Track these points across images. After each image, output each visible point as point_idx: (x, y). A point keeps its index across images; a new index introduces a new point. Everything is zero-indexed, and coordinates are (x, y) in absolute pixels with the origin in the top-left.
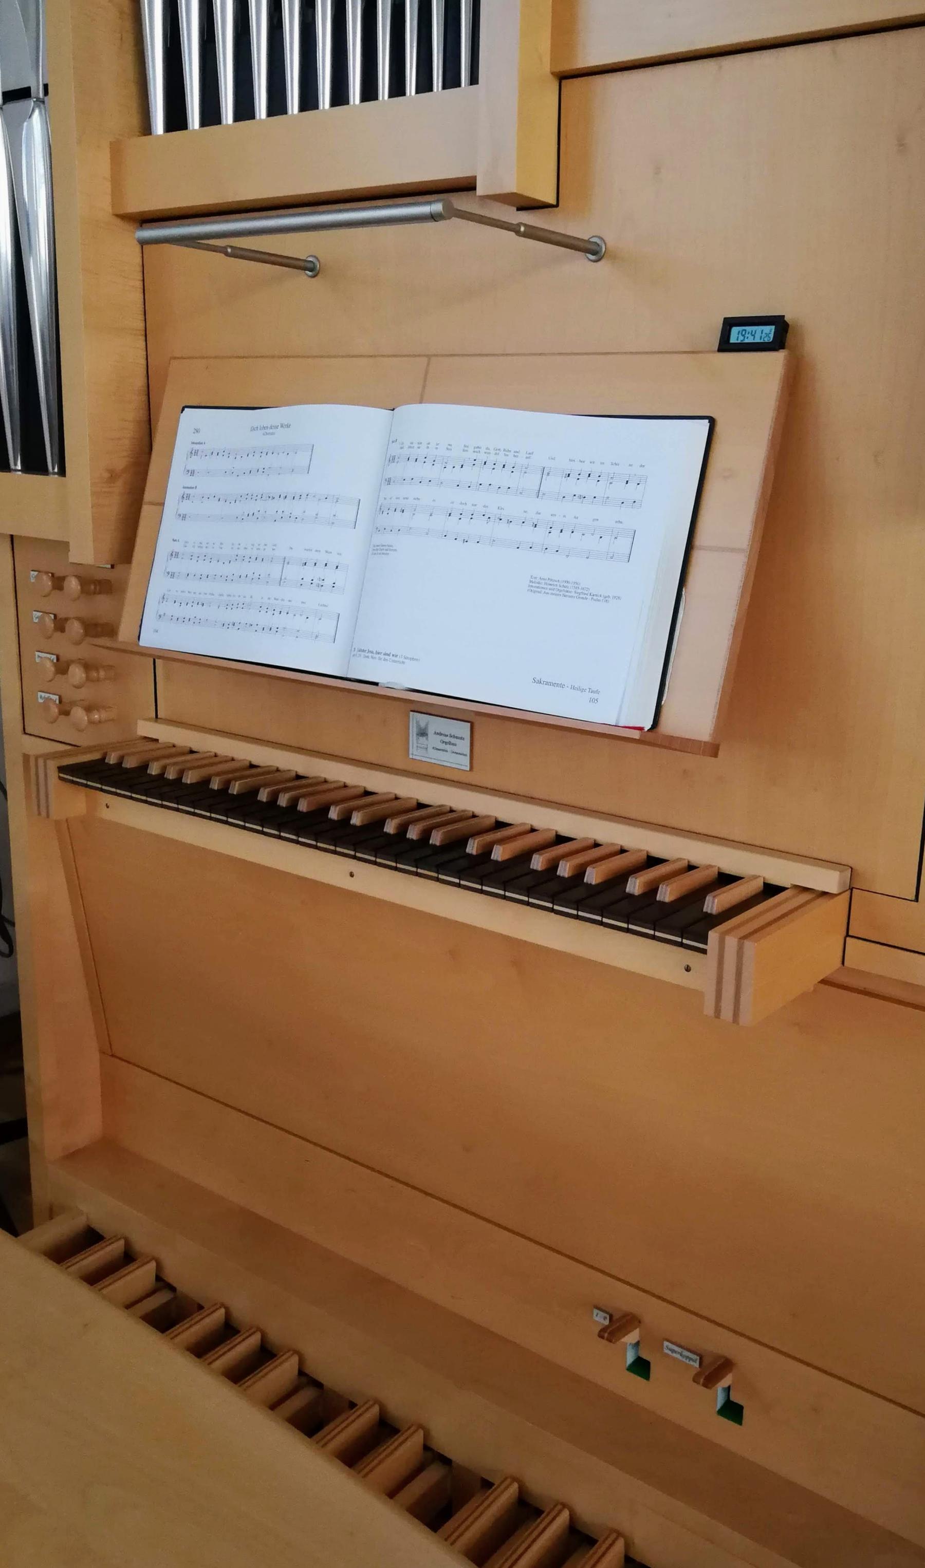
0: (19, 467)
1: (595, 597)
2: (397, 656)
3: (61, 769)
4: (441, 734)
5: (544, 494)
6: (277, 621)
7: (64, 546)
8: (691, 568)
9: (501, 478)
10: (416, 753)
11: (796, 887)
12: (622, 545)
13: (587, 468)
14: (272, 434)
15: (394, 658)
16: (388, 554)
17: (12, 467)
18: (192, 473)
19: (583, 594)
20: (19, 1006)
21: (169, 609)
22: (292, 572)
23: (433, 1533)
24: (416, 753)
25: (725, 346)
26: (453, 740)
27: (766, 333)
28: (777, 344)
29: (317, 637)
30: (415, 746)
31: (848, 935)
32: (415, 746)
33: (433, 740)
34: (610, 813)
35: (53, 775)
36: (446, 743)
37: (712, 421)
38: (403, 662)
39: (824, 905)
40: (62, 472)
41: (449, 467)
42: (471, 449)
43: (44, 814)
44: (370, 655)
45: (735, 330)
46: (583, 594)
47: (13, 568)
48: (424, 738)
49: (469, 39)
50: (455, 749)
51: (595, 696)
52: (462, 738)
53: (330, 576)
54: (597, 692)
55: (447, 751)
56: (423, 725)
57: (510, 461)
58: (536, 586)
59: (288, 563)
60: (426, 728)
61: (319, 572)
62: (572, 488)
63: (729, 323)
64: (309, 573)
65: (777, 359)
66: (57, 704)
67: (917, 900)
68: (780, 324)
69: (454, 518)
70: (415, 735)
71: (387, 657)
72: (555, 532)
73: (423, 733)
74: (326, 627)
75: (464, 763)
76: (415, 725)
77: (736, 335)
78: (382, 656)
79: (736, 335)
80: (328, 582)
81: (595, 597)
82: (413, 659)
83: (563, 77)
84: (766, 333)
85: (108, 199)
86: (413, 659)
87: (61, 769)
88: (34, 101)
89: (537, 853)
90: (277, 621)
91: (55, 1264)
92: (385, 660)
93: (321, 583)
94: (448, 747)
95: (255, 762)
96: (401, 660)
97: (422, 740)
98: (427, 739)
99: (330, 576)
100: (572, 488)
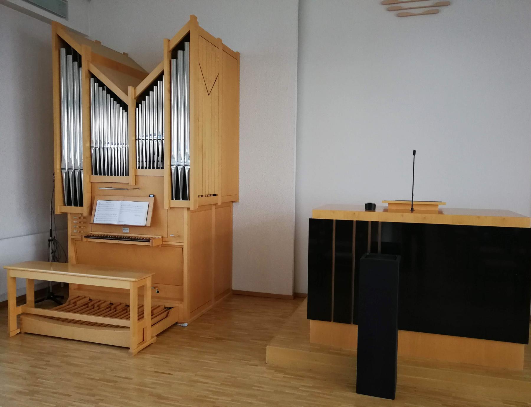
3: (84, 236)
20: (150, 73)
21: (97, 219)
22: (112, 215)
23: (349, 325)
25: (150, 197)
27: (153, 196)
28: (154, 197)
31: (163, 241)
33: (125, 230)
34: (408, 17)
35: (84, 237)
47: (89, 126)
63: (150, 195)
68: (154, 195)
75: (128, 232)
83: (135, 176)
85: (88, 180)
87: (84, 236)
89: (52, 309)
91: (8, 317)
99: (116, 215)
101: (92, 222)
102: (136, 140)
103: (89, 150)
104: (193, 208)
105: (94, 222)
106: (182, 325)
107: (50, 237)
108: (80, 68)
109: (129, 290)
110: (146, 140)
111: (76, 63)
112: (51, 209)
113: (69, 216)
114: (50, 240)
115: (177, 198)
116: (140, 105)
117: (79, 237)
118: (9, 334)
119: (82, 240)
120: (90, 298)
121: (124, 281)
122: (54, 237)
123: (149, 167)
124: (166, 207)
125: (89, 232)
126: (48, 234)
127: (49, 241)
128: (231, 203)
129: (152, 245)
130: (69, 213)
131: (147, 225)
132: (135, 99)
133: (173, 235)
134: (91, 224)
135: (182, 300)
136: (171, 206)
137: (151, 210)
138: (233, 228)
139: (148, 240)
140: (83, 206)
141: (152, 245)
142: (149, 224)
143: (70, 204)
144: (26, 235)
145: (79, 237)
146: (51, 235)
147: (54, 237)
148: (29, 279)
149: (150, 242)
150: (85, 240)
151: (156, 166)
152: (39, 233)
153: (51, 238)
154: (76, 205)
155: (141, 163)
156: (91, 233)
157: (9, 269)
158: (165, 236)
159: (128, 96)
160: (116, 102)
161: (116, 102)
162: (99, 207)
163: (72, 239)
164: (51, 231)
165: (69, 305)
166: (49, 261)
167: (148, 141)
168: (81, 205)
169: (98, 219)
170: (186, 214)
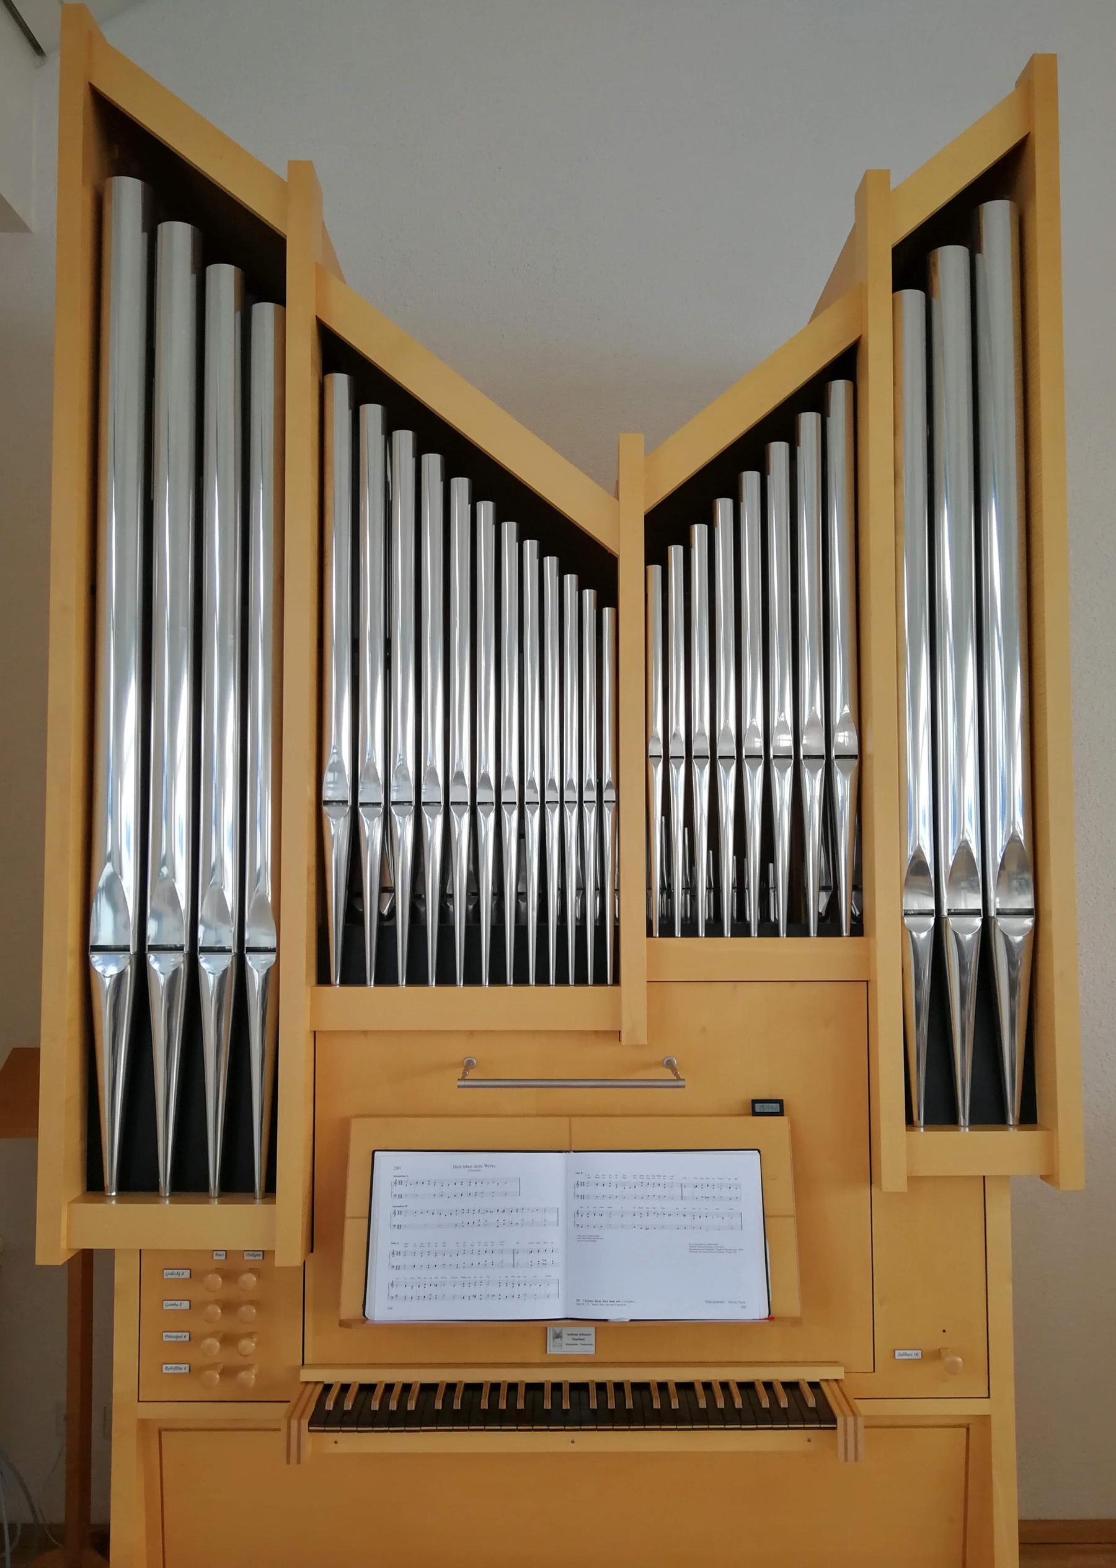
1: (729, 1251)
2: (619, 1302)
4: (572, 1334)
5: (685, 1198)
8: (306, 1221)
9: (658, 1191)
15: (618, 1303)
18: (400, 1196)
19: (721, 1250)
26: (582, 1337)
27: (775, 1107)
28: (781, 1113)
29: (548, 1296)
30: (551, 1345)
32: (551, 1345)
33: (566, 1339)
36: (577, 1339)
38: (625, 1305)
41: (627, 1188)
42: (638, 1177)
44: (598, 1303)
46: (721, 1250)
48: (559, 1339)
49: (110, 1031)
50: (583, 1342)
51: (743, 1305)
52: (590, 1335)
53: (549, 1257)
54: (744, 1302)
55: (577, 1344)
57: (662, 1181)
58: (693, 1249)
59: (518, 1253)
60: (561, 1333)
63: (754, 1102)
66: (296, 1372)
67: (874, 1371)
68: (780, 1102)
69: (638, 1216)
70: (552, 1337)
71: (612, 1303)
73: (558, 1336)
74: (553, 1289)
76: (552, 1332)
77: (758, 1108)
78: (608, 1303)
79: (758, 1108)
80: (549, 1261)
81: (729, 1251)
84: (775, 1107)
88: (204, 961)
92: (611, 1305)
93: (545, 1262)
94: (578, 1342)
96: (624, 1303)
97: (558, 1340)
98: (562, 1339)
99: (549, 1257)
116: (675, 553)
136: (923, 1170)
137: (785, 1201)
142: (791, 1305)
163: (143, 1425)
169: (408, 1292)
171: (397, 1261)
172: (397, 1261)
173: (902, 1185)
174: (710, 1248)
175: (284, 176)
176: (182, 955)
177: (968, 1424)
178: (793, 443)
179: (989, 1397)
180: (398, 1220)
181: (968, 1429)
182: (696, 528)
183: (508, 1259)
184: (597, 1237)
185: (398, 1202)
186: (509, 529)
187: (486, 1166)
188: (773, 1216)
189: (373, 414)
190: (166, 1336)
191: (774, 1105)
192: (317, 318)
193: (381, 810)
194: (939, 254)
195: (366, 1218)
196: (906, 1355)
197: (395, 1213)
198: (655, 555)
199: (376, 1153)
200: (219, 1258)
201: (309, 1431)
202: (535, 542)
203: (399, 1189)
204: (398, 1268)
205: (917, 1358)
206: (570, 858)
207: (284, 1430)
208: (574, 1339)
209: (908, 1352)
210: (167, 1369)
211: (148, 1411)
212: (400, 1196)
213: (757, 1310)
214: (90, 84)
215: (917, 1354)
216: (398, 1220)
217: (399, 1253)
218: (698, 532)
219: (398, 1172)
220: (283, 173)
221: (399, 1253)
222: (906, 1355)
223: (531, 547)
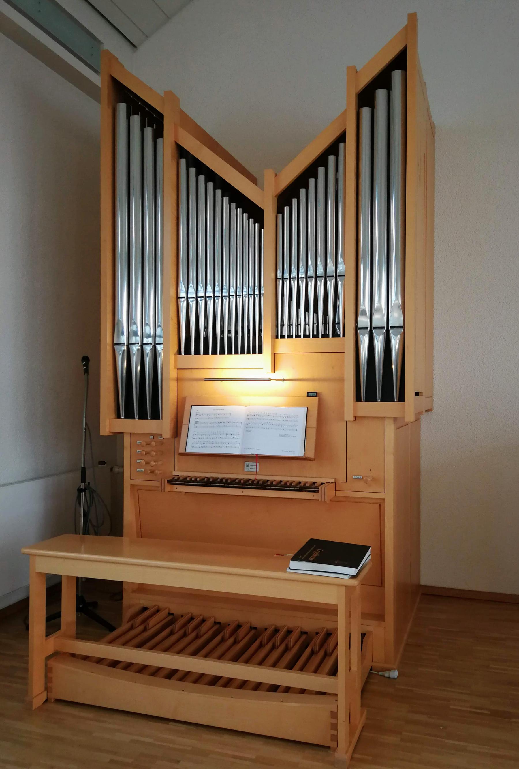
0: (137, 418)
3: (168, 481)
6: (228, 445)
7: (161, 435)
10: (246, 470)
11: (327, 483)
12: (295, 428)
13: (287, 416)
14: (219, 411)
16: (251, 431)
17: (135, 418)
18: (197, 418)
19: (289, 436)
22: (228, 436)
24: (246, 470)
25: (308, 396)
27: (315, 394)
28: (316, 396)
31: (335, 490)
33: (250, 467)
35: (166, 480)
37: (307, 408)
39: (333, 484)
40: (162, 420)
43: (163, 490)
45: (309, 394)
46: (289, 436)
56: (248, 464)
60: (248, 465)
61: (235, 436)
62: (284, 419)
63: (308, 393)
64: (232, 436)
65: (317, 398)
68: (316, 393)
72: (283, 426)
73: (248, 466)
77: (309, 394)
79: (309, 394)
80: (237, 437)
82: (258, 449)
84: (315, 394)
86: (258, 449)
87: (168, 481)
90: (228, 445)
94: (254, 468)
95: (207, 477)
99: (237, 436)
100: (284, 419)
101: (181, 450)
102: (276, 279)
103: (175, 303)
104: (352, 419)
105: (188, 451)
106: (387, 675)
107: (82, 482)
108: (159, 140)
109: (336, 606)
110: (199, 299)
111: (149, 131)
112: (84, 426)
113: (127, 440)
114: (82, 489)
115: (371, 397)
116: (287, 209)
117: (158, 484)
118: (31, 703)
119: (163, 489)
120: (215, 619)
121: (113, 563)
122: (89, 483)
123: (304, 335)
124: (349, 416)
125: (172, 472)
126: (79, 474)
127: (80, 490)
128: (311, 454)
129: (323, 500)
130: (128, 433)
131: (306, 455)
132: (276, 196)
133: (360, 477)
134: (181, 454)
135: (380, 617)
136: (360, 414)
137: (313, 422)
138: (422, 462)
139: (313, 488)
140: (404, 401)
141: (323, 500)
142: (311, 454)
143: (129, 415)
144: (31, 480)
145: (158, 484)
146: (83, 480)
147: (89, 483)
148: (68, 576)
149: (318, 492)
150: (168, 488)
151: (321, 333)
152: (49, 476)
153: (82, 486)
154: (143, 416)
155: (286, 327)
156: (174, 473)
157: (35, 555)
158: (341, 478)
159: (263, 190)
160: (234, 204)
161: (234, 204)
162: (197, 420)
163: (133, 486)
164: (83, 470)
165: (132, 628)
166: (76, 532)
167: (193, 301)
168: (156, 415)
169: (197, 445)
170: (390, 429)
171: (195, 437)
172: (195, 437)
173: (351, 418)
174: (285, 435)
175: (163, 95)
176: (139, 346)
177: (380, 503)
178: (326, 167)
179: (385, 493)
180: (196, 425)
181: (380, 505)
182: (293, 200)
183: (225, 436)
184: (251, 431)
185: (197, 420)
186: (233, 205)
187: (222, 409)
188: (309, 428)
189: (193, 171)
190: (138, 461)
191: (315, 394)
192: (175, 141)
193: (195, 299)
194: (377, 92)
195: (188, 425)
196: (357, 477)
197: (195, 423)
198: (280, 210)
199: (192, 406)
200: (151, 438)
201: (167, 483)
202: (241, 209)
203: (197, 416)
204: (195, 439)
205: (360, 478)
206: (158, 283)
207: (160, 481)
208: (252, 467)
209: (358, 476)
210: (138, 470)
211: (133, 482)
212: (197, 418)
213: (299, 453)
214: (111, 75)
215: (361, 477)
216: (196, 425)
217: (195, 435)
218: (294, 201)
219: (197, 412)
220: (163, 95)
221: (195, 435)
222: (357, 477)
223: (240, 210)
